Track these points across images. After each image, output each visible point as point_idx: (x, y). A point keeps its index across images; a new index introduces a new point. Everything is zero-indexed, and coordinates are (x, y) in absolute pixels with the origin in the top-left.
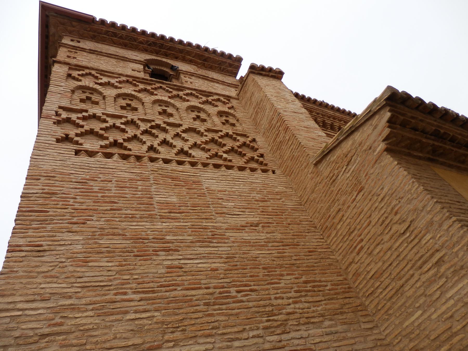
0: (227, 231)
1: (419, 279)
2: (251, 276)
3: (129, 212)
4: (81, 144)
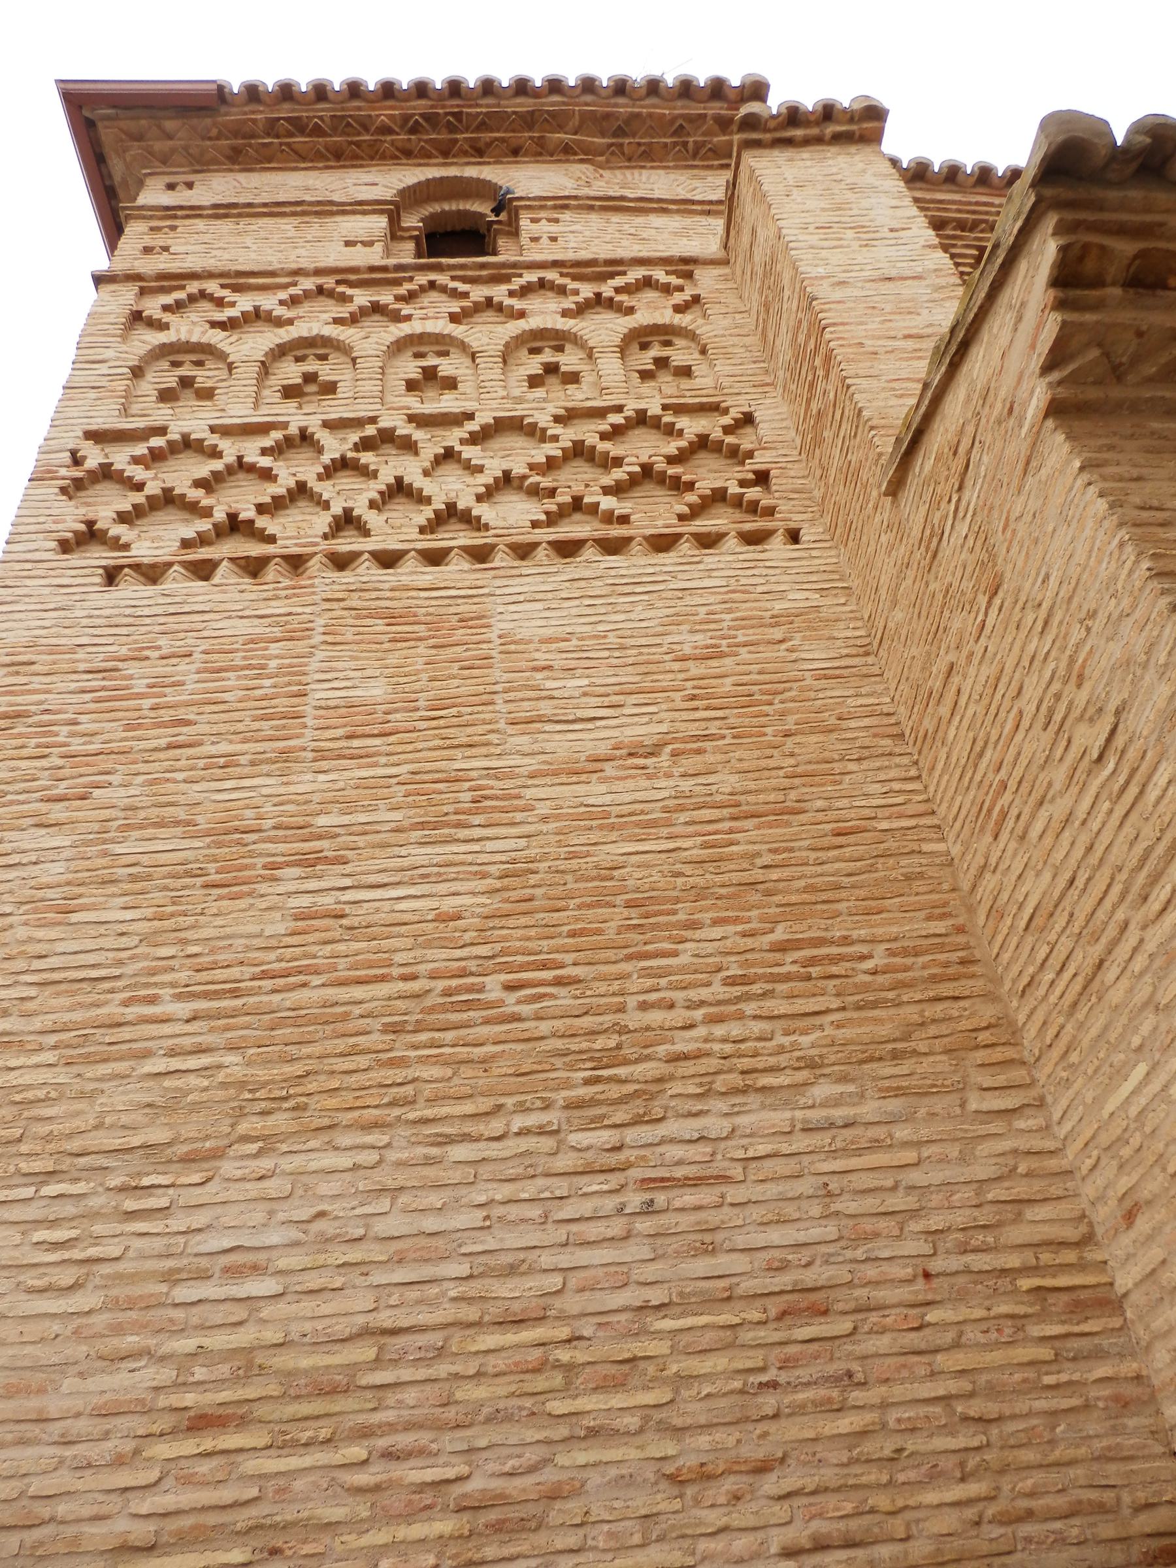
0: (530, 782)
1: (1142, 941)
2: (573, 934)
3: (224, 748)
4: (126, 547)
